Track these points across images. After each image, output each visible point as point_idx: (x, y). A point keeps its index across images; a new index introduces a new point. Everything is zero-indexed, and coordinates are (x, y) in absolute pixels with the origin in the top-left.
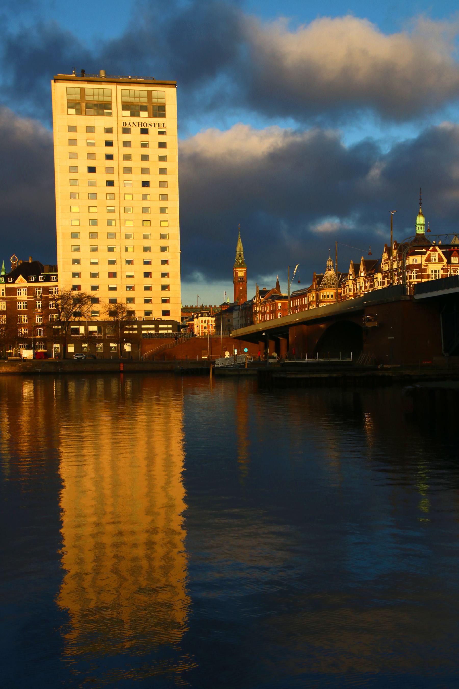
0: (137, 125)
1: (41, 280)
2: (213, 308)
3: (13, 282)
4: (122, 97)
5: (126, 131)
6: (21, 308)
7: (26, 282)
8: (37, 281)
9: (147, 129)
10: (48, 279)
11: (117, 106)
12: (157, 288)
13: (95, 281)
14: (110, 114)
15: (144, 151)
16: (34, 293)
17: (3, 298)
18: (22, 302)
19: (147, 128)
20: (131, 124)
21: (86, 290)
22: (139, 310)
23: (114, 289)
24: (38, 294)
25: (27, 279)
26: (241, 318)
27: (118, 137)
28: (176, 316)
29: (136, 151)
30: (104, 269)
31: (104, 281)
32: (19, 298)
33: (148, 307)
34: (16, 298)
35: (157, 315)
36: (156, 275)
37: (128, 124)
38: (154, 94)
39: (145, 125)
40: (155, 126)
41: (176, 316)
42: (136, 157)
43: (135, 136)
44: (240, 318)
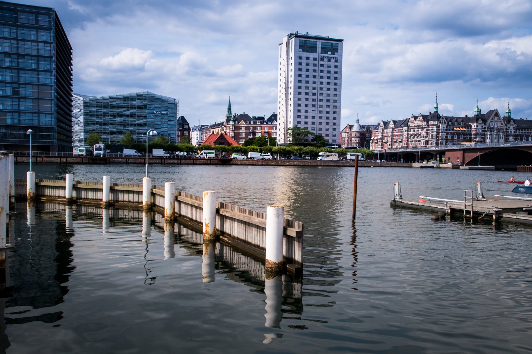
32: (241, 131)
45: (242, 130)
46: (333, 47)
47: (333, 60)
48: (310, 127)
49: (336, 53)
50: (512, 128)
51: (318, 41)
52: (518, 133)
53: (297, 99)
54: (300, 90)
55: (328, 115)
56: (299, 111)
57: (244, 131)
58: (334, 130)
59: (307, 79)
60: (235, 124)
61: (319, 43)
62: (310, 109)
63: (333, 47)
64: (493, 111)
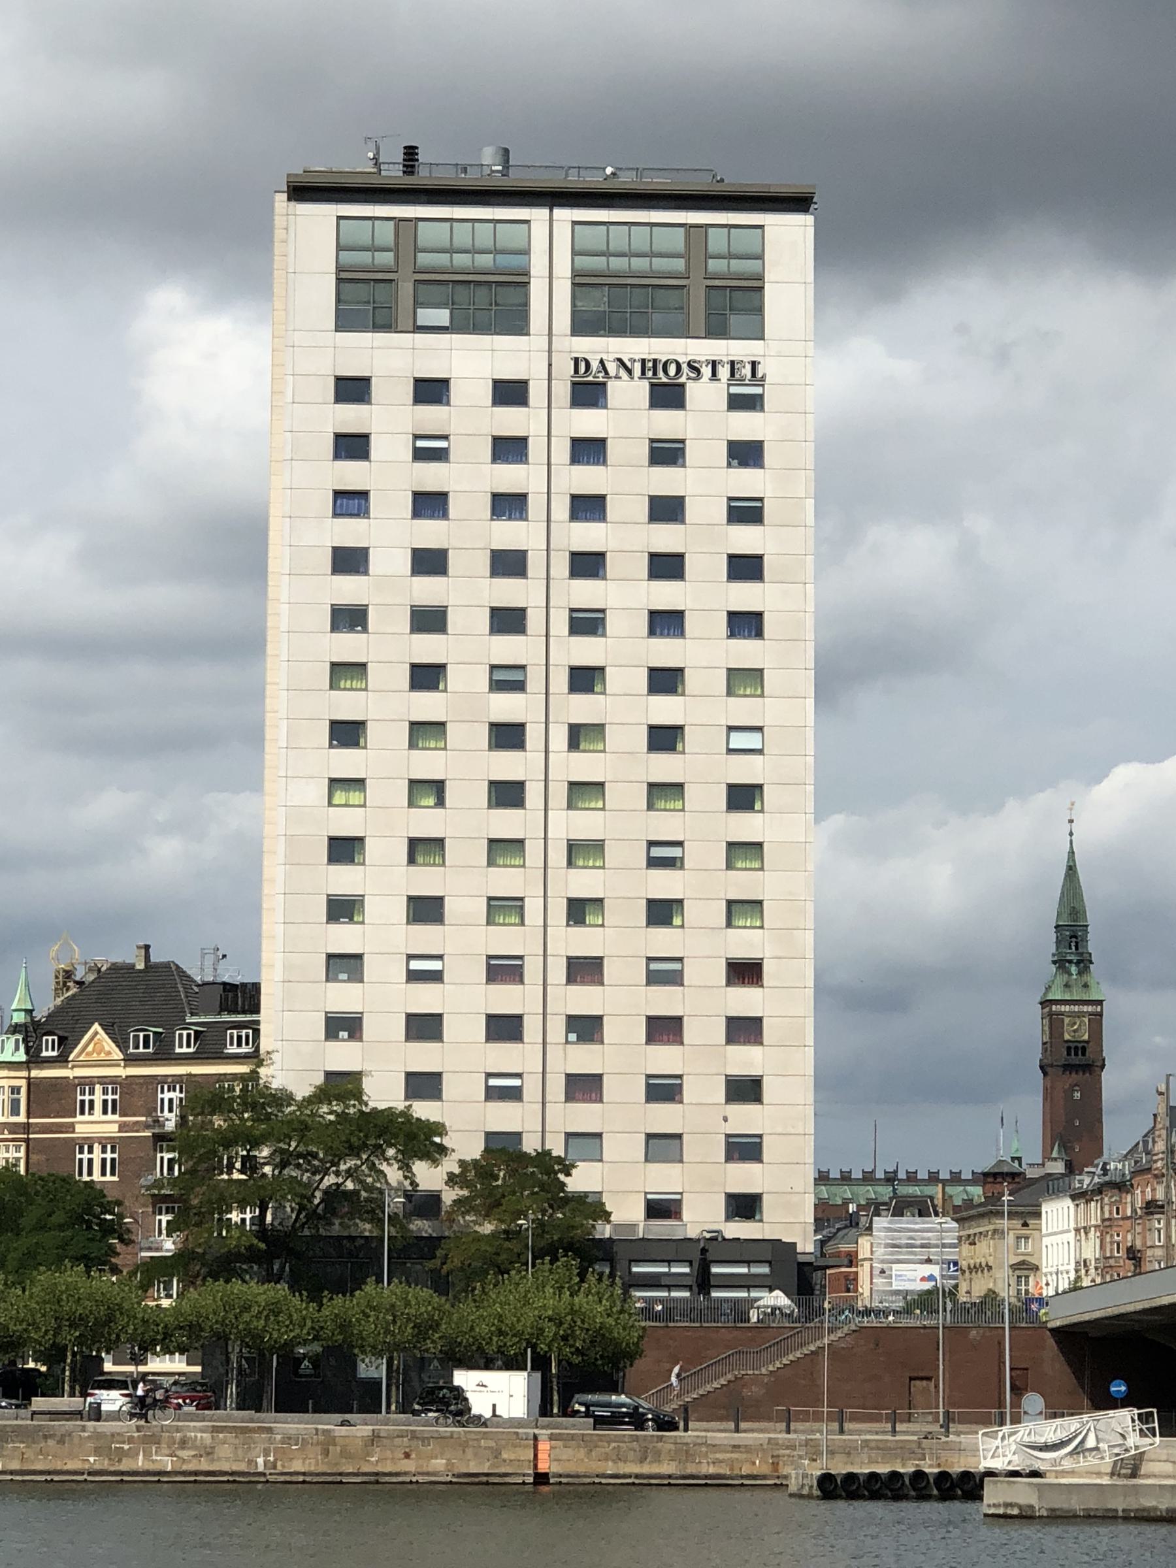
0: (637, 368)
1: (185, 1050)
2: (945, 1183)
3: (62, 1060)
4: (575, 253)
6: (90, 1173)
7: (117, 1055)
8: (164, 1055)
9: (683, 385)
10: (209, 1046)
11: (550, 296)
12: (704, 1089)
13: (424, 1057)
15: (666, 481)
16: (151, 1109)
17: (13, 1128)
18: (97, 1148)
19: (683, 380)
20: (612, 368)
21: (384, 1093)
22: (617, 1186)
24: (166, 1113)
25: (122, 1044)
26: (1082, 1230)
27: (549, 422)
28: (790, 1221)
30: (465, 1001)
31: (463, 1056)
33: (664, 1179)
34: (71, 1128)
35: (703, 1216)
36: (702, 1030)
37: (595, 365)
38: (717, 242)
39: (672, 370)
40: (714, 373)
41: (790, 1221)
42: (627, 737)
43: (627, 417)
44: (1077, 1230)
45: (96, 1124)
47: (705, 394)
51: (538, 215)
60: (34, 1059)
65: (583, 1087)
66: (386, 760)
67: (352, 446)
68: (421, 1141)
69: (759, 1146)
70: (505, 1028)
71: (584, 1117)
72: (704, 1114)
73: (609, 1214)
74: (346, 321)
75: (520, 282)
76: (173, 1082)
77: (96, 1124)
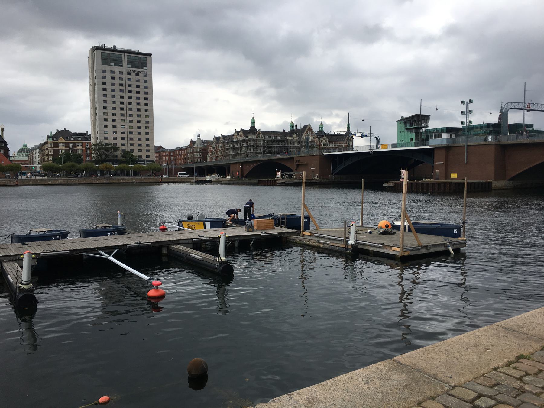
5: (129, 74)
8: (70, 140)
12: (144, 145)
14: (121, 66)
16: (69, 146)
23: (124, 145)
27: (125, 76)
29: (134, 101)
32: (60, 148)
38: (142, 59)
42: (135, 110)
43: (133, 76)
45: (62, 147)
46: (140, 61)
48: (119, 142)
49: (144, 68)
50: (324, 141)
51: (123, 54)
52: (331, 146)
53: (102, 114)
54: (146, 108)
55: (139, 130)
56: (146, 128)
57: (64, 147)
58: (148, 145)
59: (113, 93)
60: (53, 140)
61: (125, 57)
62: (118, 124)
63: (140, 61)
64: (307, 125)
65: (132, 145)
66: (110, 111)
67: (104, 77)
68: (116, 149)
69: (193, 141)
70: (123, 139)
71: (132, 148)
72: (144, 147)
73: (192, 141)
74: (103, 64)
75: (121, 61)
76: (71, 143)
77: (62, 147)
